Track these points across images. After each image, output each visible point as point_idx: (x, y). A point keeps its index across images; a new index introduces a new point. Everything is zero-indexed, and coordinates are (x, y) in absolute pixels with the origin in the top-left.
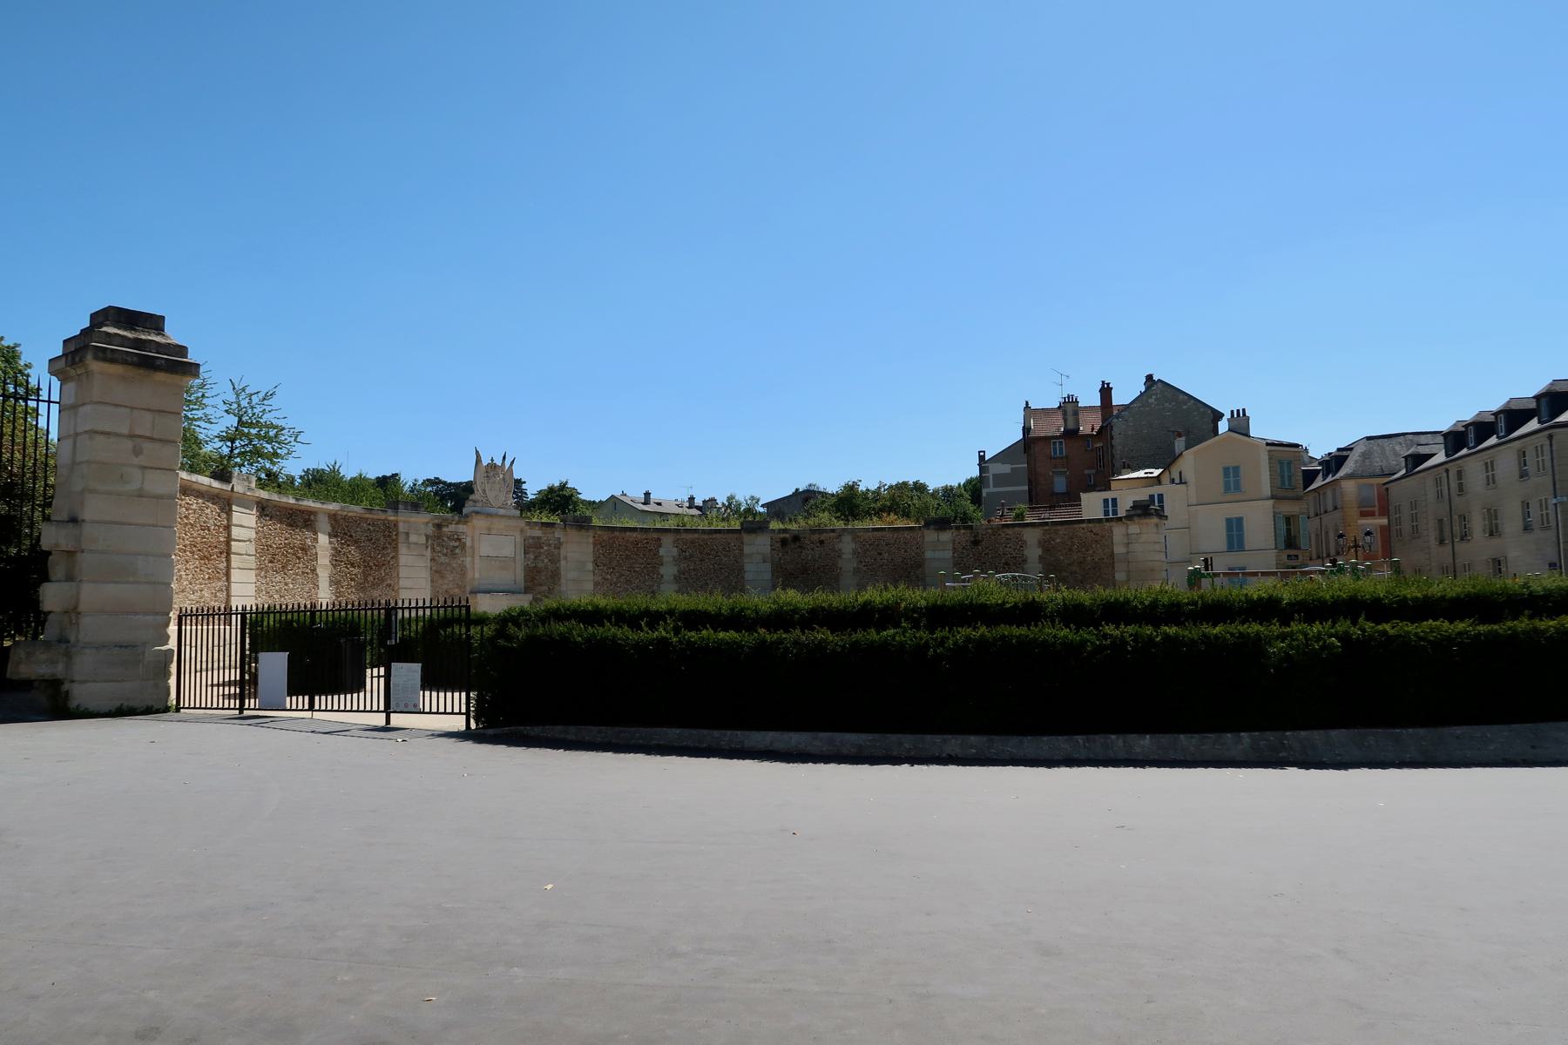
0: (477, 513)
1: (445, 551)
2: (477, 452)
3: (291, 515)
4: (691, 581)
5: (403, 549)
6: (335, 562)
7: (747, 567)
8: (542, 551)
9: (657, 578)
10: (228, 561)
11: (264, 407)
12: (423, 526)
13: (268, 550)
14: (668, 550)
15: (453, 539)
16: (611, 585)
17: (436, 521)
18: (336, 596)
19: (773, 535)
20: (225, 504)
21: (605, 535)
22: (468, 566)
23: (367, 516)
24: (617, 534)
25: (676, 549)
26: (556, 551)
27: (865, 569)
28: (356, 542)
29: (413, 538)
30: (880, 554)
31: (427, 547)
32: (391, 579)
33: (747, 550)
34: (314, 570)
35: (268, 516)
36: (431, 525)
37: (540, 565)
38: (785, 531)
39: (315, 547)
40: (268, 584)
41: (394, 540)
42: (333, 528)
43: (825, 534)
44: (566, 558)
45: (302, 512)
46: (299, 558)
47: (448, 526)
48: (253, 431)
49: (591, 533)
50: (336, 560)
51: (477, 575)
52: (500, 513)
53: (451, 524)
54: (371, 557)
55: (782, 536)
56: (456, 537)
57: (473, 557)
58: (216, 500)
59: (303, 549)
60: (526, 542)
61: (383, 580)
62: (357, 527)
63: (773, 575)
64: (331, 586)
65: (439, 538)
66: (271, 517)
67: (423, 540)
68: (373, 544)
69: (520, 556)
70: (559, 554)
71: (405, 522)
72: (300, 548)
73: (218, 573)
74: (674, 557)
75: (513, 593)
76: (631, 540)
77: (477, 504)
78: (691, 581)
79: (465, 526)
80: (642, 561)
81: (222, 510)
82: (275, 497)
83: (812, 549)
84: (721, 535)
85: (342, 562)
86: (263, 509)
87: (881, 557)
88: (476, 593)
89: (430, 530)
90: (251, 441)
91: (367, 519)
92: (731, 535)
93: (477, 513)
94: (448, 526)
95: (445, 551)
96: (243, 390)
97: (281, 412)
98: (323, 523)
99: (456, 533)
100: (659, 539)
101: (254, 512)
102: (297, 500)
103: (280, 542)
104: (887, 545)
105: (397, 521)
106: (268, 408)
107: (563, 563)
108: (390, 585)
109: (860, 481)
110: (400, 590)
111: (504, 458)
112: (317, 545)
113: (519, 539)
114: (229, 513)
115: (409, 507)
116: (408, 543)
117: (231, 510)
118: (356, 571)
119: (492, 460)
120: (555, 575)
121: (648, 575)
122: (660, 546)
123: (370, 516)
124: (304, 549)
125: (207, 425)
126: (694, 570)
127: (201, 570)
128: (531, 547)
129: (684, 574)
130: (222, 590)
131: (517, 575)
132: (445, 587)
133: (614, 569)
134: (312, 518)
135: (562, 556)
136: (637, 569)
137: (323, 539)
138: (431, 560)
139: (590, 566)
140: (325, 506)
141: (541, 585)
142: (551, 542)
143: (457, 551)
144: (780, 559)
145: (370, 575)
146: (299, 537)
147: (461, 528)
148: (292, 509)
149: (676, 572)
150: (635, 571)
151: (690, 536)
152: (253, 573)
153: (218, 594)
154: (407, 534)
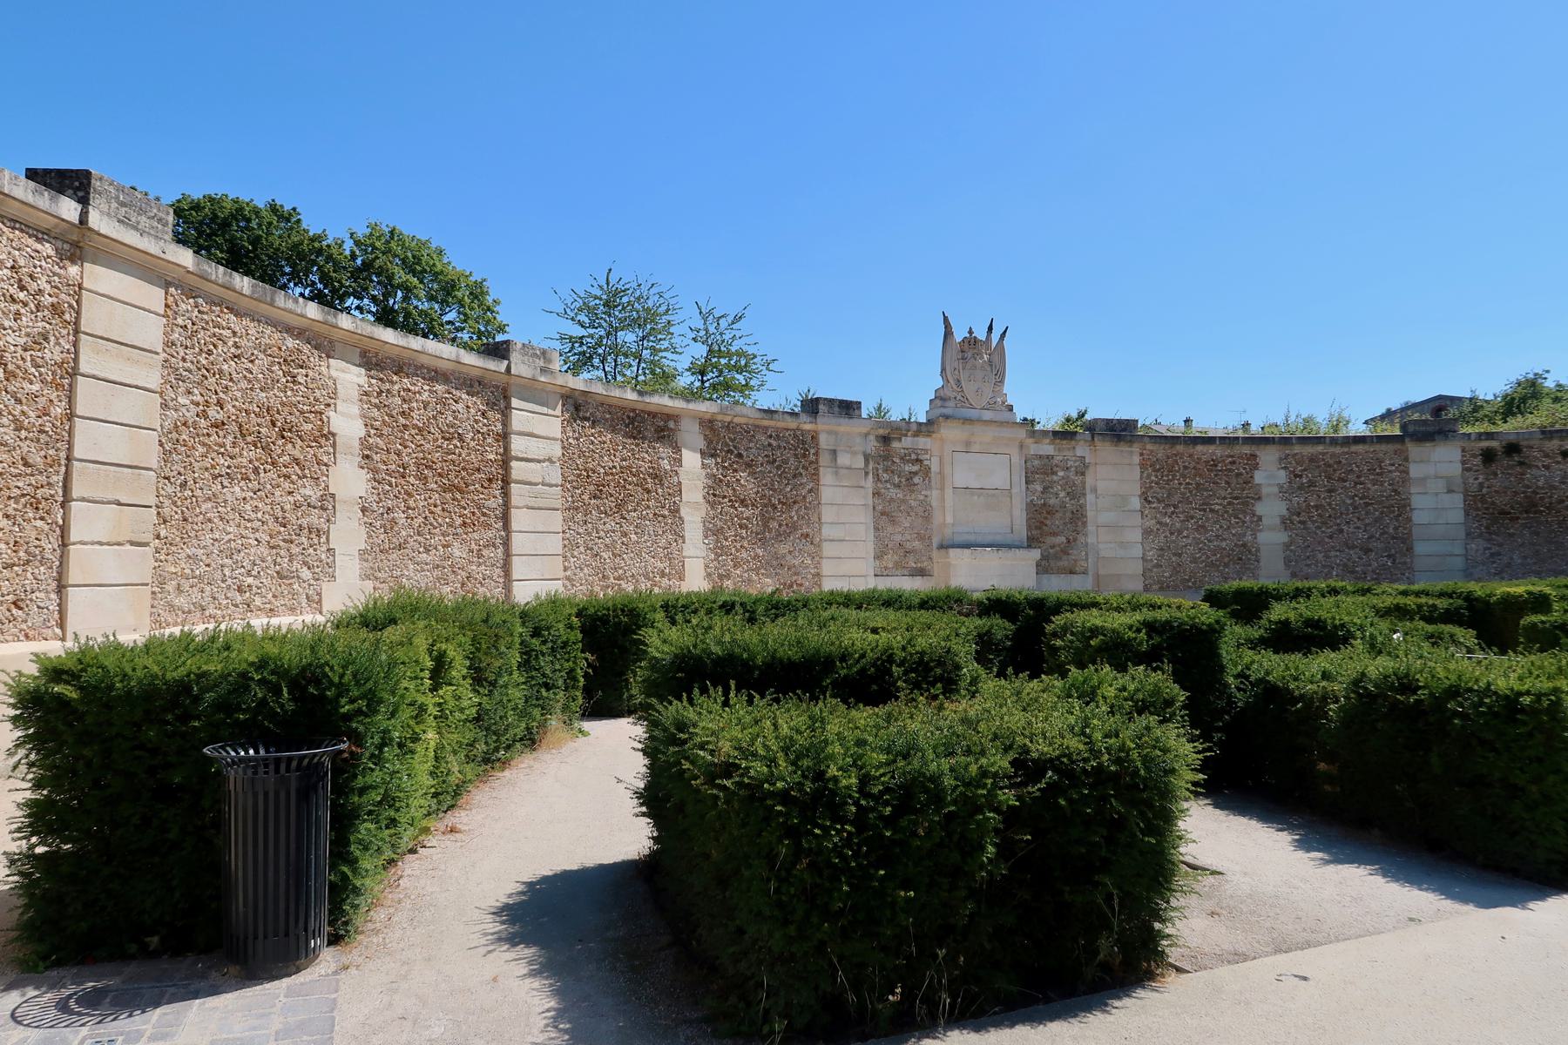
0: (947, 417)
2: (946, 319)
3: (632, 420)
4: (1310, 524)
5: (826, 477)
6: (714, 495)
7: (1417, 501)
8: (1055, 478)
9: (1252, 522)
10: (506, 494)
11: (734, 332)
13: (588, 477)
14: (1269, 474)
15: (908, 461)
16: (1172, 534)
17: (881, 432)
18: (716, 554)
19: (1466, 444)
20: (499, 396)
21: (1161, 451)
22: (934, 504)
23: (766, 423)
24: (1180, 448)
25: (1283, 473)
26: (1078, 479)
28: (749, 465)
29: (843, 459)
31: (867, 474)
32: (808, 525)
33: (1415, 471)
34: (675, 511)
35: (587, 419)
36: (872, 437)
37: (1052, 501)
38: (1489, 436)
39: (677, 473)
40: (589, 534)
41: (811, 463)
42: (710, 442)
44: (1094, 490)
45: (653, 415)
46: (648, 492)
47: (900, 440)
48: (723, 361)
49: (1136, 448)
50: (714, 495)
51: (949, 520)
53: (906, 435)
54: (774, 490)
55: (1485, 444)
56: (914, 456)
57: (942, 489)
58: (477, 388)
59: (655, 477)
61: (795, 527)
62: (750, 441)
63: (1467, 514)
64: (706, 537)
65: (886, 458)
66: (594, 422)
67: (859, 462)
68: (778, 468)
69: (1019, 487)
70: (1084, 483)
72: (650, 475)
73: (484, 515)
74: (1280, 486)
75: (1010, 547)
76: (1204, 458)
77: (947, 404)
78: (1310, 524)
79: (928, 439)
80: (1223, 493)
81: (491, 405)
83: (1547, 467)
84: (1366, 447)
85: (725, 497)
86: (577, 408)
88: (948, 547)
89: (872, 445)
90: (721, 372)
91: (766, 428)
92: (1384, 447)
93: (947, 417)
94: (900, 440)
96: (710, 313)
97: (751, 338)
98: (691, 434)
100: (1254, 456)
101: (558, 411)
102: (641, 393)
103: (611, 464)
105: (815, 432)
106: (738, 334)
107: (1090, 498)
109: (1548, 372)
110: (825, 544)
111: (990, 328)
112: (680, 471)
113: (1017, 459)
114: (506, 412)
115: (836, 409)
116: (837, 469)
117: (508, 407)
118: (747, 513)
119: (971, 332)
120: (1077, 518)
121: (1236, 517)
122: (1256, 467)
123: (772, 423)
124: (657, 476)
125: (674, 357)
126: (1317, 507)
127: (443, 510)
129: (1298, 514)
130: (494, 545)
131: (1013, 518)
132: (898, 538)
133: (1175, 507)
134: (671, 424)
135: (1088, 486)
136: (1217, 507)
137: (691, 460)
139: (1136, 503)
140: (692, 406)
141: (1055, 534)
142: (1070, 463)
143: (916, 480)
145: (773, 519)
146: (647, 456)
148: (634, 410)
149: (1285, 512)
150: (1212, 511)
151: (1309, 450)
152: (558, 516)
153: (485, 552)
154: (834, 452)
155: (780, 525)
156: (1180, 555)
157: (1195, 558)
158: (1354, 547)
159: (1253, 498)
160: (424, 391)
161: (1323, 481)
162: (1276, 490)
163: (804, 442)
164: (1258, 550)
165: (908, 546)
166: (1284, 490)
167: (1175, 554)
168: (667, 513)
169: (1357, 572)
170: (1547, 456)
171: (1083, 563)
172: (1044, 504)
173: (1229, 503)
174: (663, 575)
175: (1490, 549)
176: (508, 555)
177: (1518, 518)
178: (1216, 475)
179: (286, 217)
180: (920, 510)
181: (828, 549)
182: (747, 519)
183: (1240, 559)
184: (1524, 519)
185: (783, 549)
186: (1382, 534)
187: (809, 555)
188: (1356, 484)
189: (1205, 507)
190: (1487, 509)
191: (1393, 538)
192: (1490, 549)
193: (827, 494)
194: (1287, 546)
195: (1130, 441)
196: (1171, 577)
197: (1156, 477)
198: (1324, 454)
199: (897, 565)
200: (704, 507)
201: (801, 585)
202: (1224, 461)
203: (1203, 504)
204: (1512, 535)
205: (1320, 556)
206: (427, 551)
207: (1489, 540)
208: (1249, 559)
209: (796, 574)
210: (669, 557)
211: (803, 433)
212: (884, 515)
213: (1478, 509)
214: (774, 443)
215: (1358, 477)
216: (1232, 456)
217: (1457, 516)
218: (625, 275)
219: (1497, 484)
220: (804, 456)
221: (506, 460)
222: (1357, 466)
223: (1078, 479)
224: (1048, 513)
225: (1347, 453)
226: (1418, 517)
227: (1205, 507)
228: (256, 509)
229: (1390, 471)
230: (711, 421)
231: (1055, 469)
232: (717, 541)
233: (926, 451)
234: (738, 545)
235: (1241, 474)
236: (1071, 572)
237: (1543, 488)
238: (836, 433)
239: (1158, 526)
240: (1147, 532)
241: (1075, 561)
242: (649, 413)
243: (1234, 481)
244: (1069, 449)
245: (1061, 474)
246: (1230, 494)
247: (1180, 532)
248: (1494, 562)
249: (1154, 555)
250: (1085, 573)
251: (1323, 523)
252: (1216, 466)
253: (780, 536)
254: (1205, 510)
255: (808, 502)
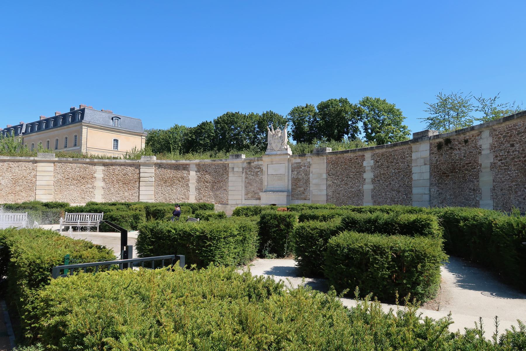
1: (253, 174)
5: (231, 174)
6: (199, 180)
7: (414, 170)
8: (301, 169)
12: (240, 164)
15: (257, 168)
16: (337, 186)
17: (248, 161)
21: (334, 157)
25: (372, 161)
27: (499, 163)
29: (236, 170)
30: (512, 145)
31: (243, 173)
32: (225, 187)
33: (414, 156)
34: (187, 185)
36: (245, 163)
37: (300, 177)
43: (468, 134)
44: (312, 172)
45: (183, 165)
46: (180, 181)
52: (278, 154)
54: (216, 179)
55: (438, 140)
56: (258, 167)
60: (293, 166)
61: (222, 187)
65: (250, 168)
70: (309, 170)
71: (232, 163)
78: (381, 181)
80: (353, 171)
82: (131, 161)
87: (513, 149)
89: (245, 165)
95: (253, 174)
99: (258, 165)
100: (364, 156)
102: (176, 161)
104: (518, 134)
107: (311, 175)
108: (225, 189)
112: (189, 176)
115: (234, 157)
118: (208, 184)
120: (307, 182)
122: (364, 160)
128: (296, 168)
131: (286, 183)
132: (253, 189)
133: (338, 176)
136: (352, 176)
138: (245, 178)
139: (325, 176)
140: (191, 162)
141: (300, 187)
143: (259, 173)
144: (437, 160)
145: (215, 186)
147: (260, 163)
148: (177, 164)
149: (373, 177)
150: (350, 177)
155: (217, 187)
156: (339, 194)
157: (344, 195)
158: (394, 191)
159: (363, 172)
160: (118, 168)
161: (386, 163)
162: (370, 168)
163: (225, 166)
164: (363, 192)
165: (256, 191)
166: (373, 168)
167: (337, 194)
168: (185, 185)
169: (395, 201)
170: (460, 143)
171: (308, 196)
172: (297, 178)
173: (355, 174)
174: (183, 199)
175: (439, 191)
176: (139, 195)
177: (449, 176)
178: (351, 164)
179: (344, 102)
180: (260, 182)
181: (230, 193)
182: (208, 186)
183: (358, 195)
184: (451, 176)
185: (218, 193)
186: (403, 185)
187: (225, 194)
188: (396, 164)
189: (348, 176)
190: (438, 172)
191: (407, 186)
192: (439, 191)
193: (230, 179)
194: (373, 190)
195: (322, 155)
196: (336, 202)
197: (332, 166)
198: (386, 152)
199: (252, 197)
200: (196, 184)
201: (223, 202)
202: (354, 158)
203: (347, 175)
204: (446, 184)
205: (383, 194)
206: (119, 194)
207: (438, 187)
208: (360, 195)
209: (221, 199)
210: (185, 195)
211: (225, 164)
212: (248, 184)
213: (435, 172)
214: (217, 167)
215: (397, 160)
216: (356, 157)
217: (427, 176)
218: (447, 93)
219: (442, 159)
220: (225, 170)
221: (139, 178)
222: (397, 156)
223: (308, 169)
224: (298, 181)
225: (394, 151)
226: (415, 177)
227: (348, 176)
228: (77, 189)
229: (407, 157)
230: (199, 164)
231: (301, 167)
232: (199, 191)
233: (262, 165)
234: (205, 192)
235: (359, 163)
236: (305, 199)
237: (458, 160)
238: (234, 163)
239: (333, 184)
240: (328, 186)
241: (306, 196)
242: (181, 165)
243: (357, 166)
244: (305, 160)
245: (303, 168)
246: (355, 171)
247: (340, 186)
248: (440, 197)
249: (331, 194)
250: (309, 200)
251: (385, 181)
252: (351, 160)
253: (217, 190)
254: (347, 177)
255: (226, 181)
